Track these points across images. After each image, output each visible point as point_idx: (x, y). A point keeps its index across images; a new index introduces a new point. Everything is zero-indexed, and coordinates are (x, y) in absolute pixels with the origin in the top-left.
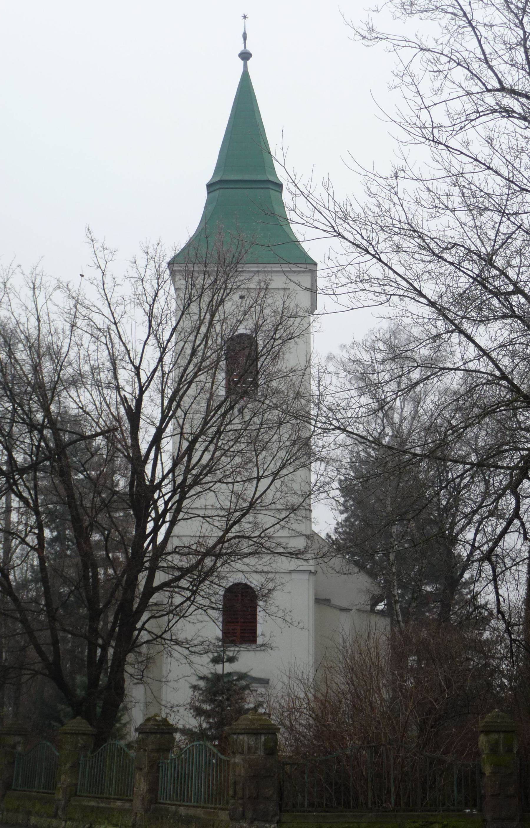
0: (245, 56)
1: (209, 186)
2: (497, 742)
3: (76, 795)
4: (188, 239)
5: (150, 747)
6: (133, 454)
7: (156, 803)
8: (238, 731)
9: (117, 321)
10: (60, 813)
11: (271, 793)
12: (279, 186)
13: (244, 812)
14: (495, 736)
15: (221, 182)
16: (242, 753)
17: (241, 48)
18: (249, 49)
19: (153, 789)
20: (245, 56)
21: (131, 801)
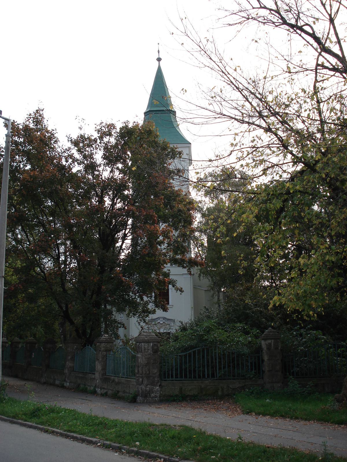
0: (159, 60)
1: (145, 113)
2: (270, 344)
3: (73, 371)
4: (171, 94)
5: (102, 349)
6: (212, 458)
7: (106, 375)
8: (139, 341)
9: (247, 17)
10: (66, 379)
11: (156, 371)
12: (174, 113)
13: (142, 381)
14: (269, 341)
15: (150, 111)
16: (141, 352)
17: (157, 57)
18: (160, 57)
19: (104, 369)
20: (159, 60)
21: (94, 374)
